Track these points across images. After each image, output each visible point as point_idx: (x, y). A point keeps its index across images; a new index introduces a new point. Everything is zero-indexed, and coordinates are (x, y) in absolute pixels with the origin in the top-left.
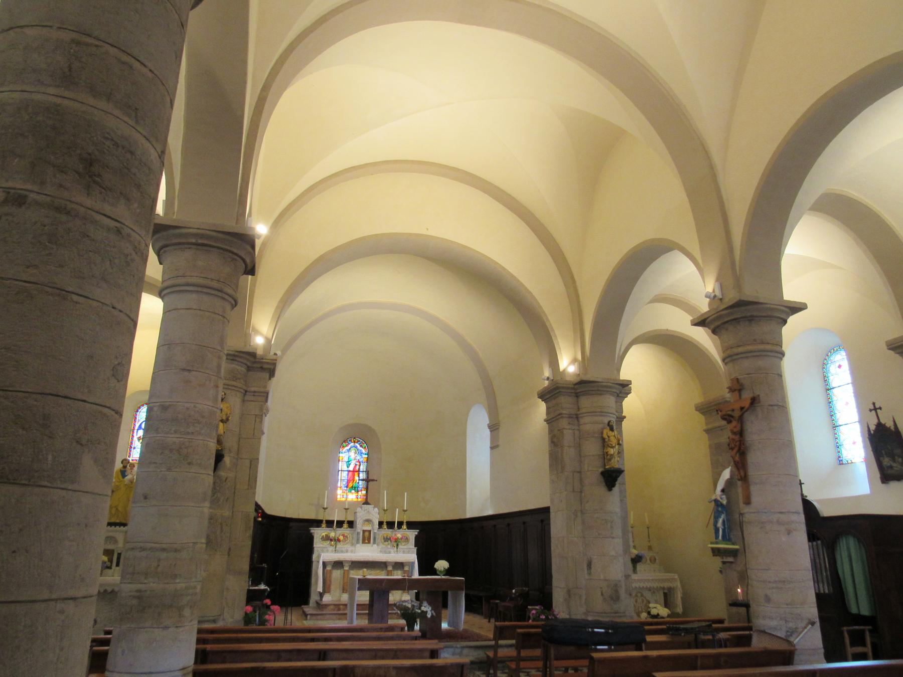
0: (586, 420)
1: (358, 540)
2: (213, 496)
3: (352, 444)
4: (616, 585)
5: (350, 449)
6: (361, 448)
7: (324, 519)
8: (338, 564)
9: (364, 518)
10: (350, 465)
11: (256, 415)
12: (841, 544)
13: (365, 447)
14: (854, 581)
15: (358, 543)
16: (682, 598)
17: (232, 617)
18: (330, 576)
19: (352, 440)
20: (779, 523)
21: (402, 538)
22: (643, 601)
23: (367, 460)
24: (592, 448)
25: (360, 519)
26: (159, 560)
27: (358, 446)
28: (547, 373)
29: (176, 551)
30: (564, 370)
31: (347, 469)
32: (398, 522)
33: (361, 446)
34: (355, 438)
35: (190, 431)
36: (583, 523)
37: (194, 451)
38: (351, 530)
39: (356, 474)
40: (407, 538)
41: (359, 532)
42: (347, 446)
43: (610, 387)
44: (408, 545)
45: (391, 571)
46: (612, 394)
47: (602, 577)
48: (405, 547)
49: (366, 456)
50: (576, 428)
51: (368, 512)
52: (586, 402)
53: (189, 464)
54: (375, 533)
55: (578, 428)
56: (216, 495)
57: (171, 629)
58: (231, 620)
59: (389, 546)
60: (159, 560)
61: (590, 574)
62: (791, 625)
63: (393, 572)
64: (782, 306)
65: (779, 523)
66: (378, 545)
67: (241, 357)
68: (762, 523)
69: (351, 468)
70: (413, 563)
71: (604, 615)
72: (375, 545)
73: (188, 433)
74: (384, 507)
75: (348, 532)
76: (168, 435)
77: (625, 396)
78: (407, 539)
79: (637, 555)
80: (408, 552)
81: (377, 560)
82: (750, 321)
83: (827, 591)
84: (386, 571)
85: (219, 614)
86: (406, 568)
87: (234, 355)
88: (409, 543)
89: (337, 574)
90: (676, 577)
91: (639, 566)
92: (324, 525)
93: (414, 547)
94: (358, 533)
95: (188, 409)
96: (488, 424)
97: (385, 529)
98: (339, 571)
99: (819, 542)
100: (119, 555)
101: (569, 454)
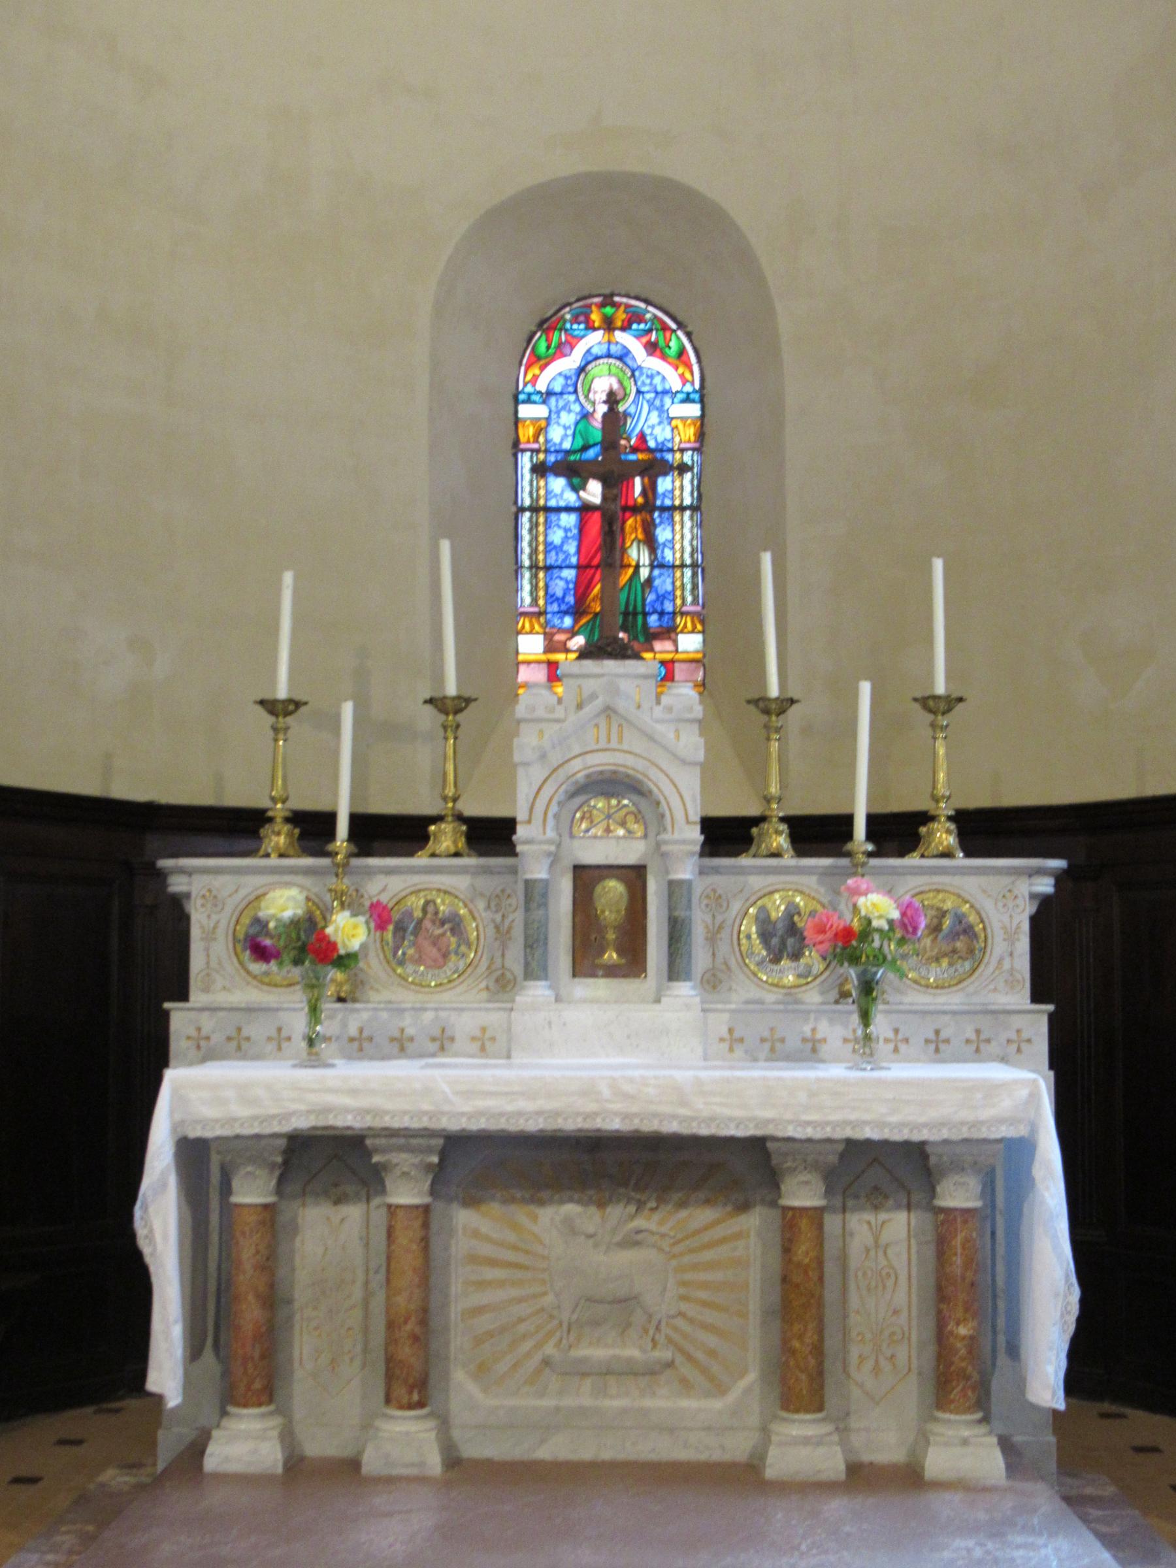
1: (535, 942)
3: (594, 340)
5: (582, 370)
6: (653, 363)
7: (279, 810)
9: (579, 769)
13: (682, 352)
15: (535, 969)
18: (270, 1262)
19: (595, 317)
21: (906, 925)
23: (701, 435)
25: (538, 773)
27: (637, 349)
32: (871, 819)
33: (652, 348)
34: (608, 300)
38: (487, 871)
40: (968, 931)
41: (412, 933)
42: (561, 351)
44: (972, 985)
45: (816, 1214)
48: (952, 1000)
49: (694, 410)
51: (609, 711)
54: (675, 889)
59: (812, 997)
63: (832, 1222)
66: (713, 982)
72: (684, 990)
74: (438, 677)
75: (461, 883)
80: (977, 1049)
81: (672, 1127)
84: (774, 1214)
88: (987, 969)
92: (278, 837)
93: (1021, 998)
94: (536, 895)
97: (777, 855)
98: (353, 1212)
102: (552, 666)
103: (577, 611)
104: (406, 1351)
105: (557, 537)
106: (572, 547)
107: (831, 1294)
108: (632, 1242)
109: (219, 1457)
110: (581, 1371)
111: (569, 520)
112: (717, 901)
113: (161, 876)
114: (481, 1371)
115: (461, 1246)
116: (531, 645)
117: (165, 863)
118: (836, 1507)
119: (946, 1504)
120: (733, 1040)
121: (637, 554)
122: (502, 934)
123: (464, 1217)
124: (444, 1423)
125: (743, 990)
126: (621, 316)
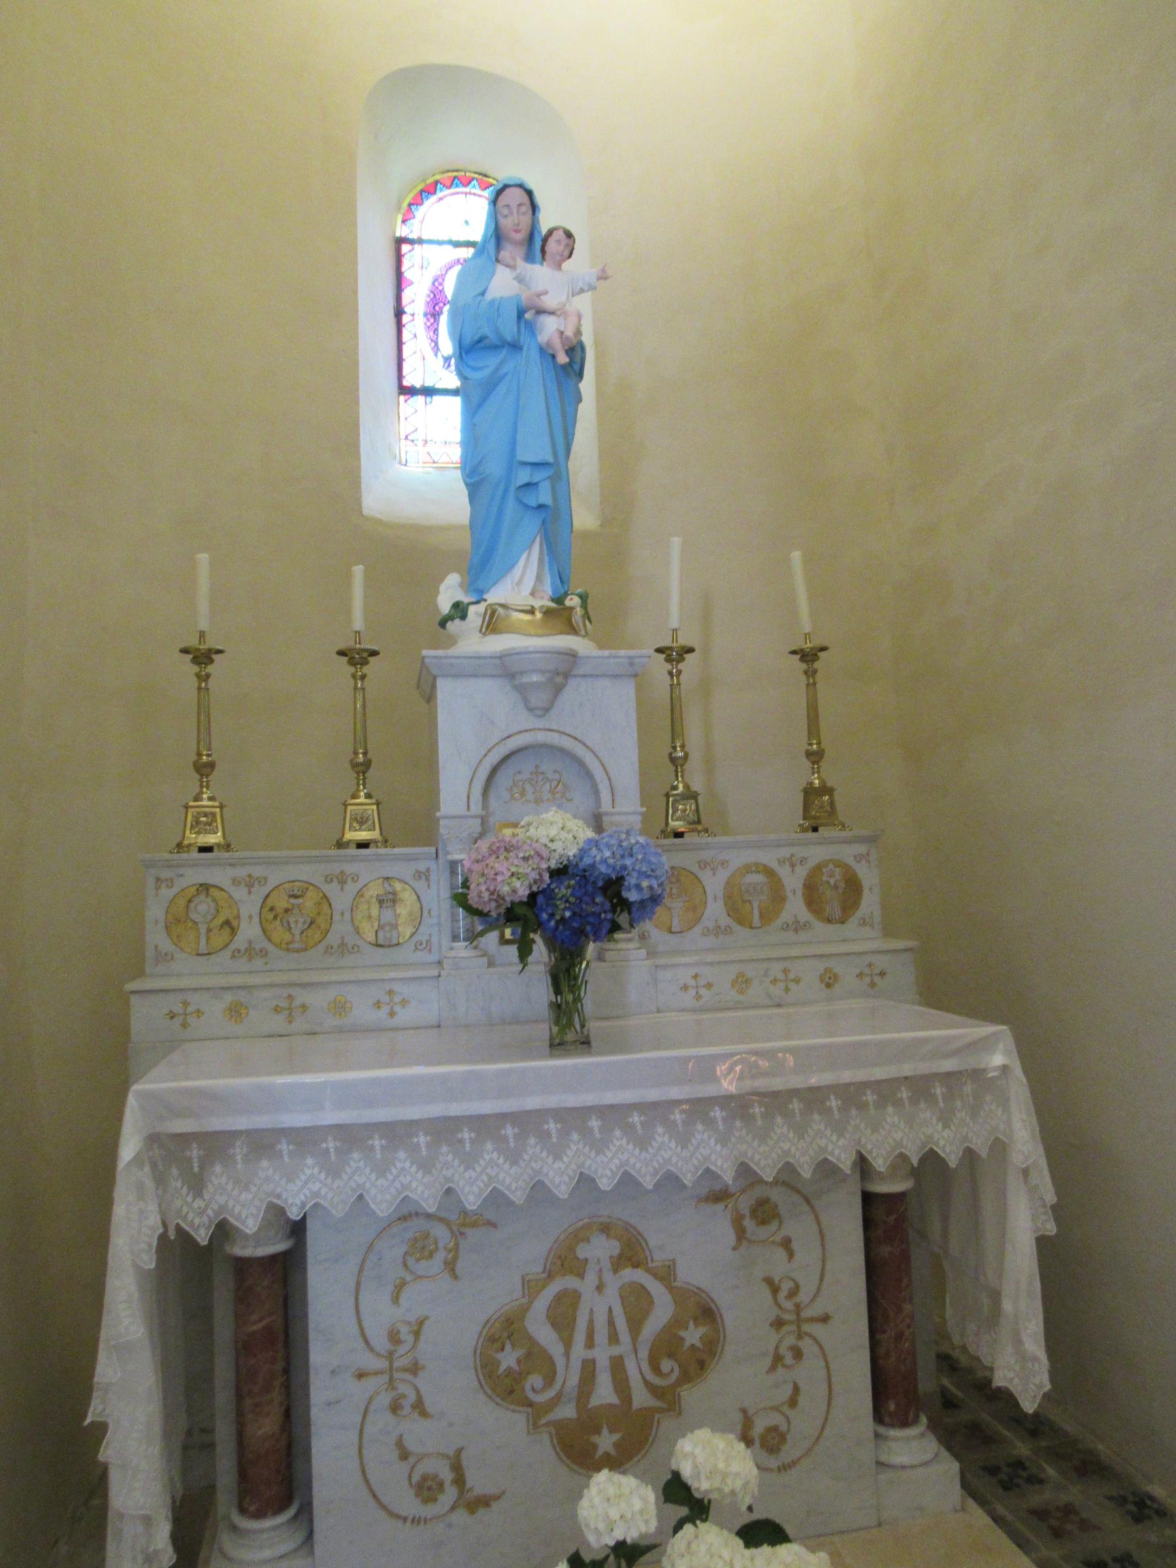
16: (1043, 1243)
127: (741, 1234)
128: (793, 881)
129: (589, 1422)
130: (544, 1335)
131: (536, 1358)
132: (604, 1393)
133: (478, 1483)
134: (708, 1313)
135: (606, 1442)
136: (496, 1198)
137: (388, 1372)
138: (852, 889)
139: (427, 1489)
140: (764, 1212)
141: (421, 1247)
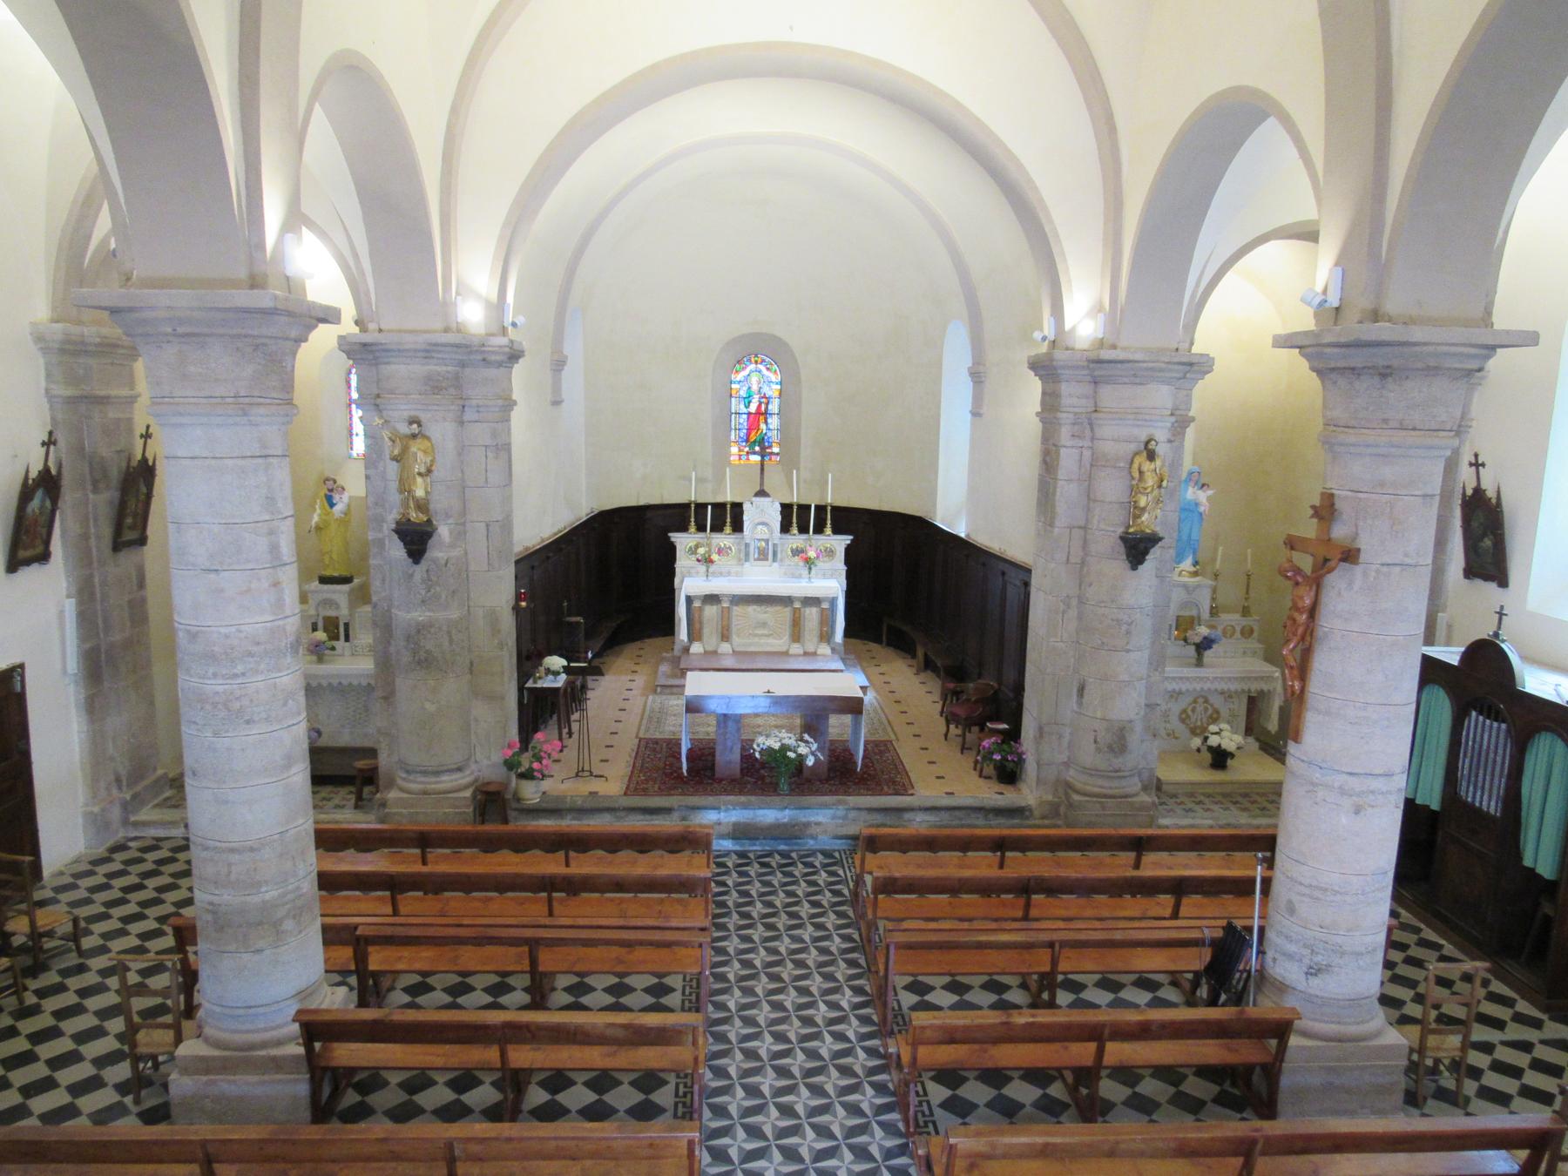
0: (1107, 430)
1: (747, 555)
2: (429, 591)
3: (752, 367)
4: (1122, 729)
8: (712, 599)
9: (756, 521)
10: (749, 403)
11: (486, 446)
12: (1541, 744)
14: (1543, 812)
16: (1281, 708)
17: (489, 758)
20: (1342, 791)
22: (1206, 709)
23: (780, 394)
24: (1111, 488)
26: (230, 865)
27: (765, 371)
28: (1048, 329)
29: (252, 849)
30: (1073, 330)
31: (745, 411)
33: (768, 369)
34: (756, 355)
35: (239, 672)
36: (1080, 618)
37: (251, 701)
39: (762, 418)
42: (744, 369)
43: (1161, 370)
45: (799, 609)
46: (1167, 382)
47: (1099, 715)
49: (779, 387)
50: (1087, 443)
51: (762, 510)
52: (1110, 396)
53: (248, 722)
54: (775, 545)
55: (1090, 444)
56: (433, 591)
57: (267, 952)
58: (486, 762)
60: (230, 865)
61: (1080, 704)
62: (1319, 958)
64: (1464, 345)
65: (1342, 791)
67: (439, 352)
68: (1313, 784)
69: (753, 408)
70: (833, 601)
71: (1093, 772)
72: (775, 564)
73: (236, 676)
76: (206, 681)
77: (1199, 376)
78: (830, 553)
79: (1205, 638)
82: (1383, 376)
83: (1492, 811)
85: (466, 757)
86: (825, 605)
87: (427, 351)
89: (711, 611)
90: (1277, 674)
91: (1208, 654)
94: (747, 545)
95: (227, 636)
96: (969, 368)
98: (715, 607)
99: (1504, 726)
100: (347, 625)
101: (1067, 492)
102: (740, 456)
103: (747, 440)
104: (725, 632)
105: (741, 421)
106: (745, 424)
107: (802, 623)
108: (765, 613)
109: (692, 650)
110: (756, 635)
111: (745, 416)
112: (783, 545)
113: (669, 538)
114: (738, 636)
115: (734, 613)
116: (734, 450)
117: (670, 534)
118: (801, 658)
119: (819, 658)
120: (785, 574)
121: (763, 426)
122: (740, 550)
123: (735, 608)
124: (732, 645)
125: (787, 562)
126: (759, 360)
127: (1225, 700)
128: (1238, 629)
129: (1196, 727)
130: (1190, 713)
131: (1188, 717)
132: (1199, 723)
133: (1177, 735)
134: (1217, 712)
135: (1198, 731)
136: (1188, 690)
137: (368, 1014)
138: (1252, 631)
139: (1168, 735)
140: (1230, 697)
141: (1172, 696)
